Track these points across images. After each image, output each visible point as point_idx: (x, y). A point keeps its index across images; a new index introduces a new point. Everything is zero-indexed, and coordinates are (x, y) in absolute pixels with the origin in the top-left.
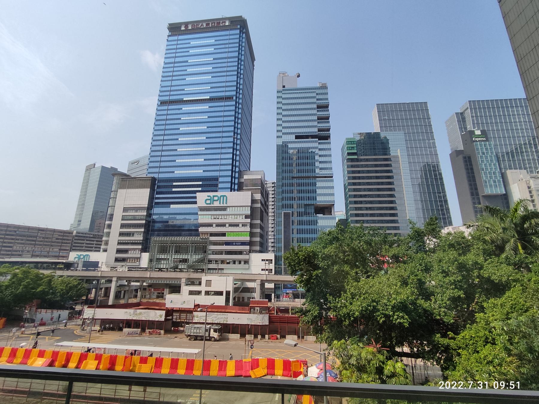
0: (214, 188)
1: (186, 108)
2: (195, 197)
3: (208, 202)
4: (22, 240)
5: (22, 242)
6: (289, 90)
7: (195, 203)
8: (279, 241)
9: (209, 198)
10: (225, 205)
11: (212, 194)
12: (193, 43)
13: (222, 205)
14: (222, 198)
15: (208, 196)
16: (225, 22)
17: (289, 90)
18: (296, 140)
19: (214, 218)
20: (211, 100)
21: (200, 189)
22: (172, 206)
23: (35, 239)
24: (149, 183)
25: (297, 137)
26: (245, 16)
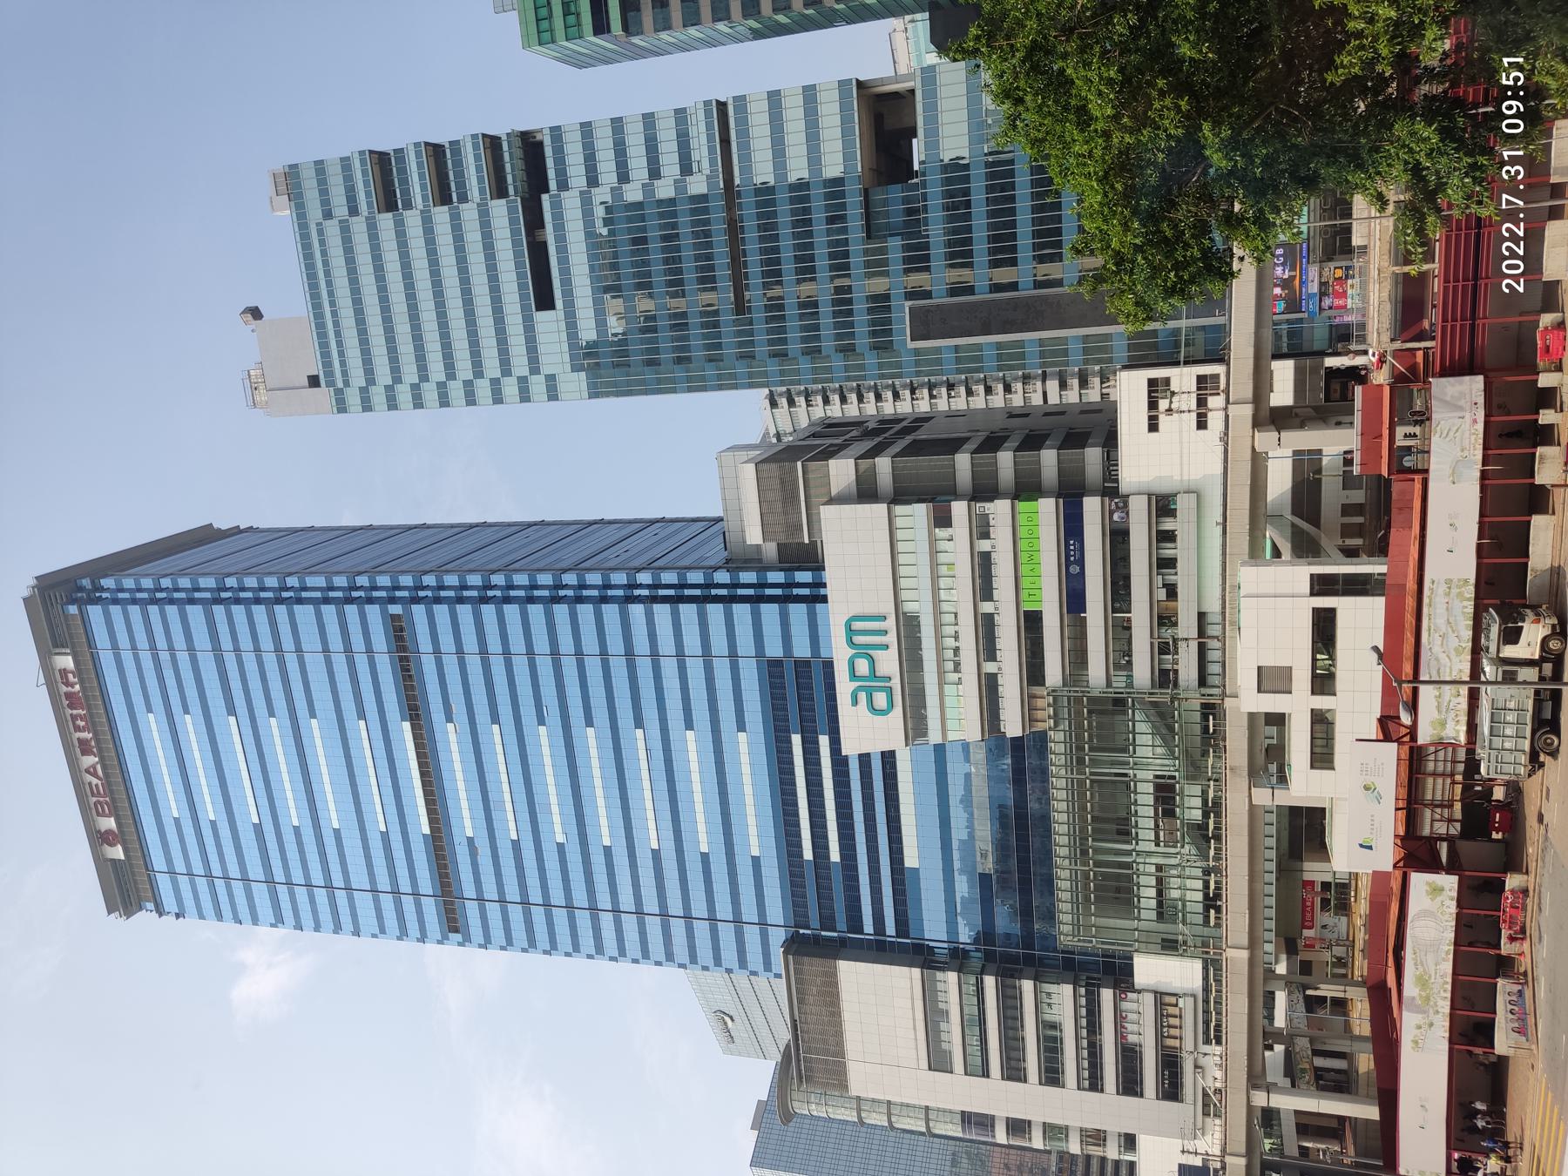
1: (465, 821)
2: (865, 759)
3: (881, 699)
7: (889, 758)
9: (863, 696)
10: (890, 624)
11: (844, 687)
13: (892, 638)
14: (859, 639)
15: (855, 702)
16: (64, 672)
19: (957, 669)
20: (415, 711)
21: (824, 741)
22: (911, 860)
24: (813, 965)
25: (545, 300)
26: (24, 585)
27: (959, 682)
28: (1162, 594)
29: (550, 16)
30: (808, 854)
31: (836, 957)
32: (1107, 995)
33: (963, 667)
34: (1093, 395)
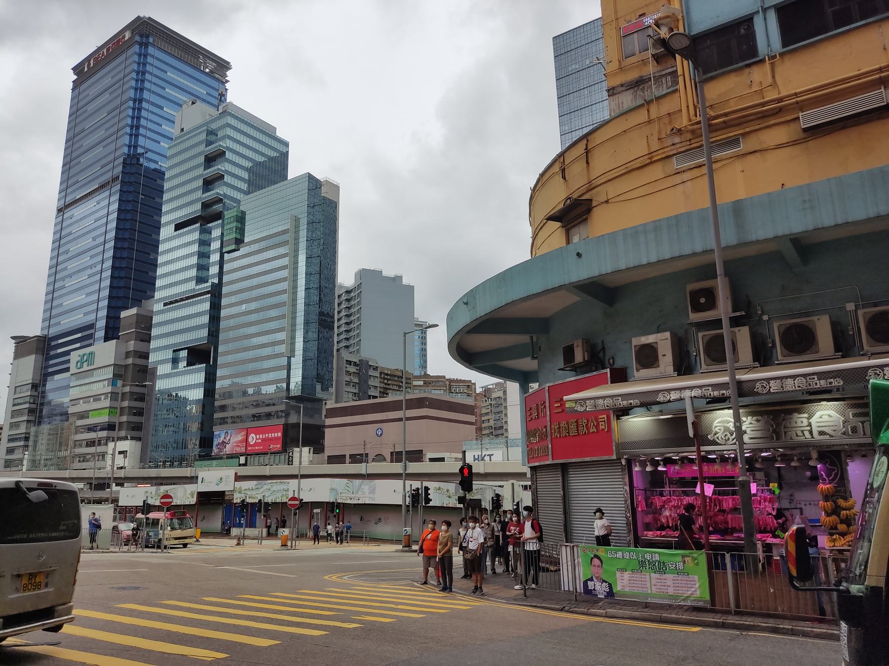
0: (91, 341)
16: (124, 37)
21: (78, 345)
22: (57, 377)
30: (60, 341)
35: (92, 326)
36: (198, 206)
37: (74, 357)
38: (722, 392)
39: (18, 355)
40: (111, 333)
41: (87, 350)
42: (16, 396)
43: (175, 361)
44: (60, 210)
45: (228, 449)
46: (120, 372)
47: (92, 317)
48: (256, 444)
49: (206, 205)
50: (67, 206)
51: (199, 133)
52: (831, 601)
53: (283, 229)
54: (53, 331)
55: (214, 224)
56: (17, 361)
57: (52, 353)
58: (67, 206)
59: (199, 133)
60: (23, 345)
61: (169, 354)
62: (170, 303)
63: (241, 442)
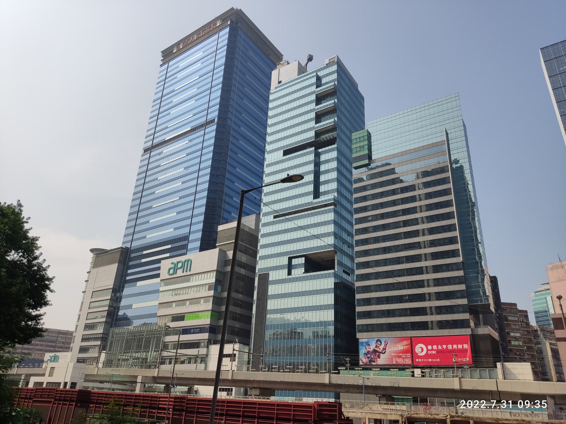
0: (184, 251)
1: (167, 150)
4: (41, 345)
5: (41, 348)
6: (286, 84)
7: (158, 276)
8: (291, 335)
12: (182, 65)
16: (216, 24)
17: (286, 84)
18: (285, 157)
19: (176, 295)
20: (193, 130)
21: (168, 255)
22: (139, 283)
23: (54, 344)
24: (117, 256)
25: (286, 153)
26: (237, 6)
27: (172, 295)
28: (182, 359)
29: (360, 142)
30: (145, 252)
31: (120, 262)
32: (99, 343)
33: (176, 296)
34: (551, 322)
35: (186, 238)
36: (312, 134)
37: (166, 265)
38: (282, 316)
39: (96, 264)
40: (208, 243)
41: (183, 258)
42: (92, 300)
43: (290, 268)
44: (146, 151)
45: (382, 360)
46: (222, 278)
47: (186, 231)
48: (427, 356)
49: (318, 134)
50: (153, 147)
51: (310, 78)
52: (22, 349)
53: (435, 141)
54: (136, 244)
55: (324, 149)
56: (96, 269)
57: (131, 263)
58: (153, 147)
59: (310, 78)
60: (100, 256)
61: (284, 261)
62: (279, 216)
63: (404, 352)
